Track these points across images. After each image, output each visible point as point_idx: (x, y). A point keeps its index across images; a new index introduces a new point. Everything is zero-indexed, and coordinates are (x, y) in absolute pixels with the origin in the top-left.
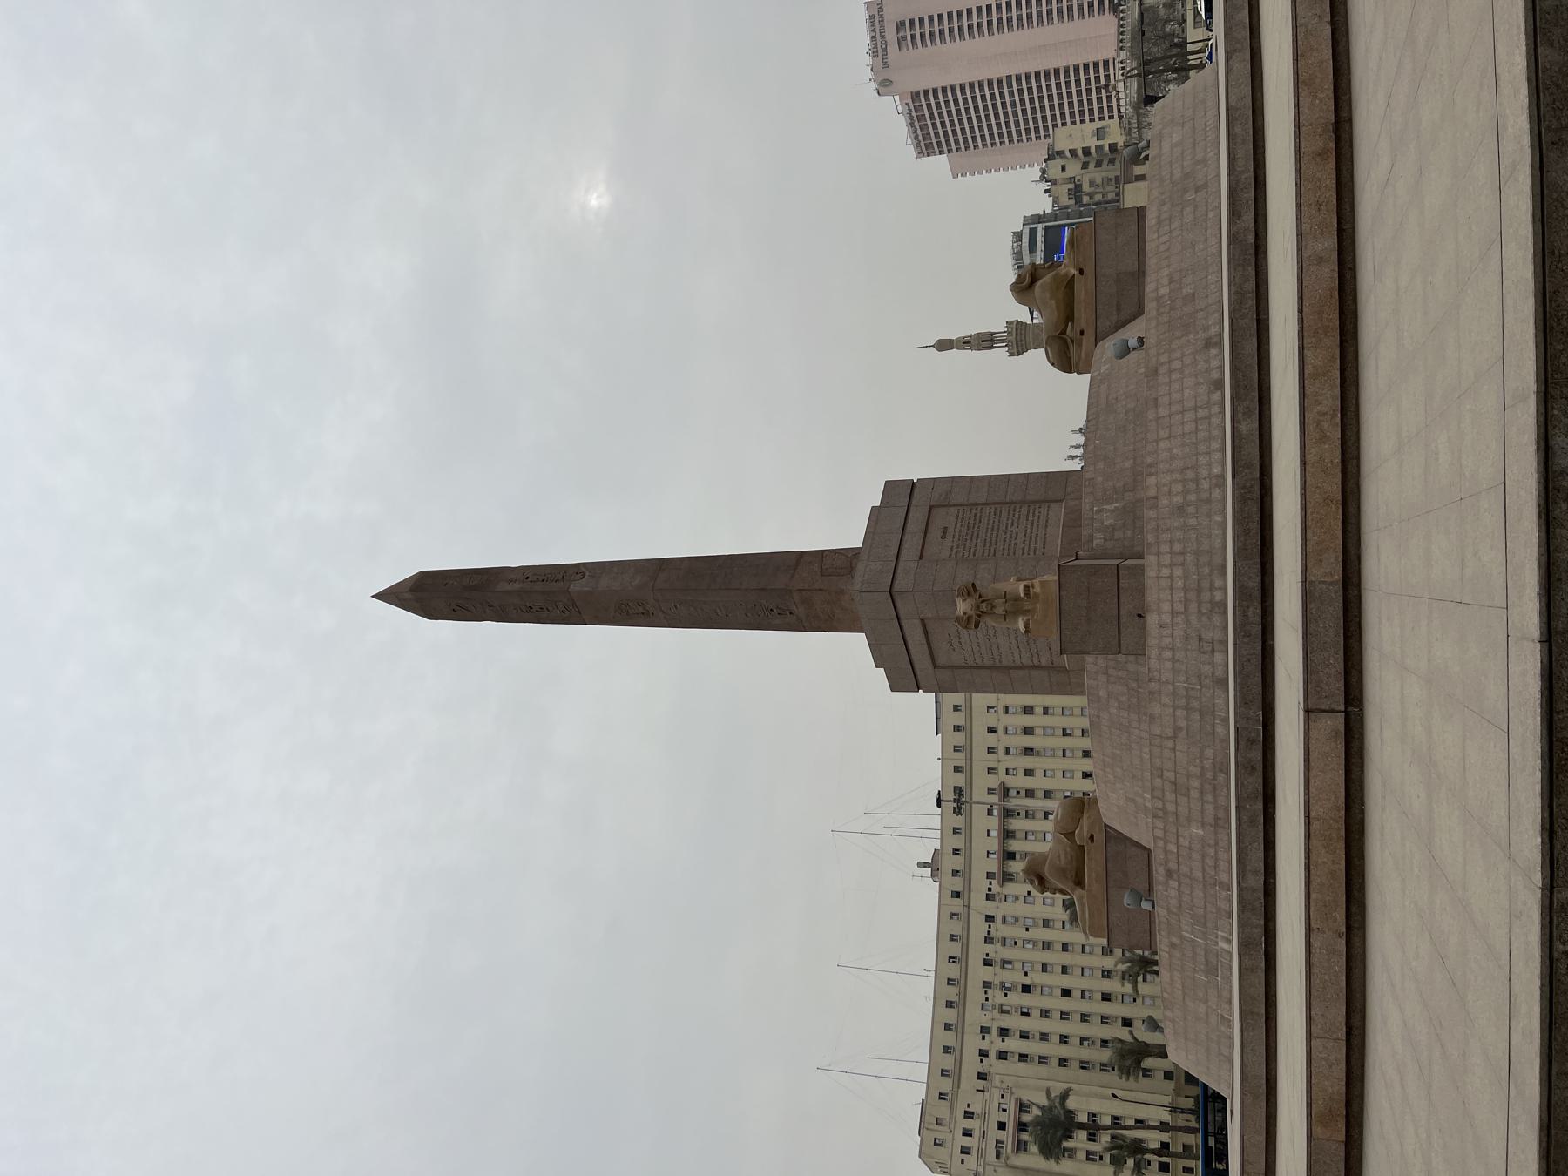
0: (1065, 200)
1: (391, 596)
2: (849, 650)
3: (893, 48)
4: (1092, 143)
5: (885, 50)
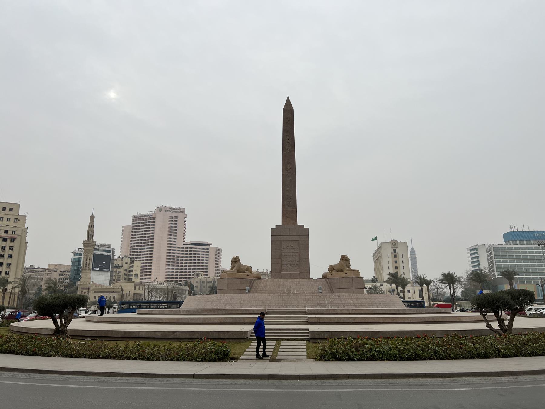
0: (115, 263)
2: (279, 222)
3: (170, 214)
4: (134, 273)
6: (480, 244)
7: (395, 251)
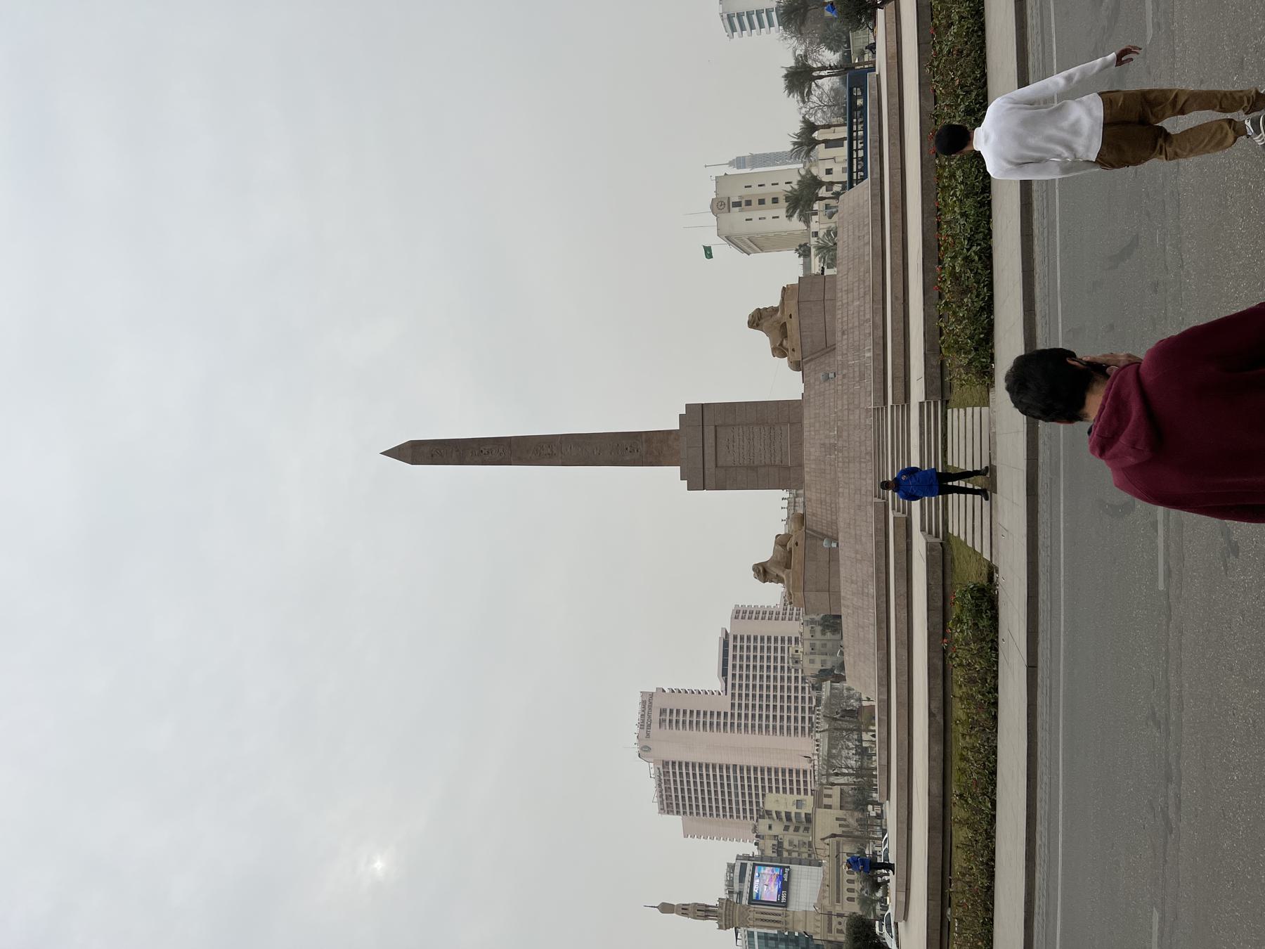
1: (391, 453)
2: (672, 473)
3: (655, 725)
4: (793, 810)
5: (649, 726)
7: (737, 204)
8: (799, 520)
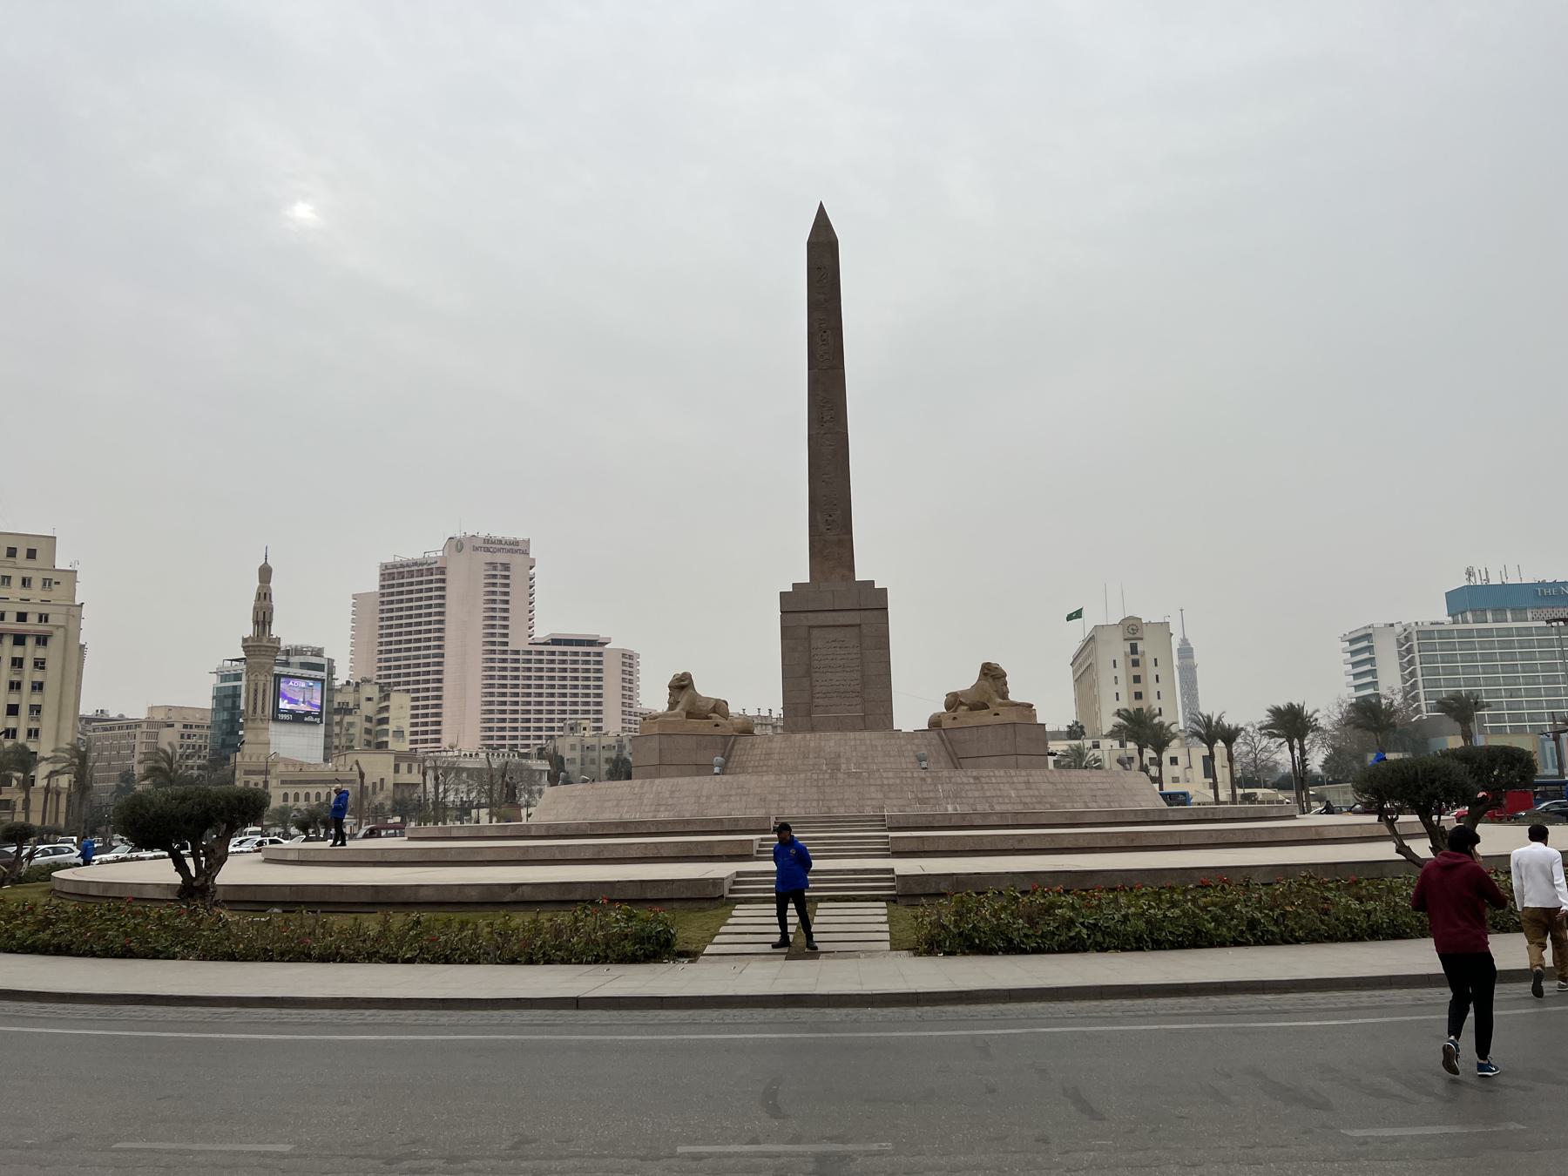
3: (489, 557)
4: (391, 727)
5: (488, 550)
6: (1379, 620)
7: (1134, 649)
8: (746, 728)
